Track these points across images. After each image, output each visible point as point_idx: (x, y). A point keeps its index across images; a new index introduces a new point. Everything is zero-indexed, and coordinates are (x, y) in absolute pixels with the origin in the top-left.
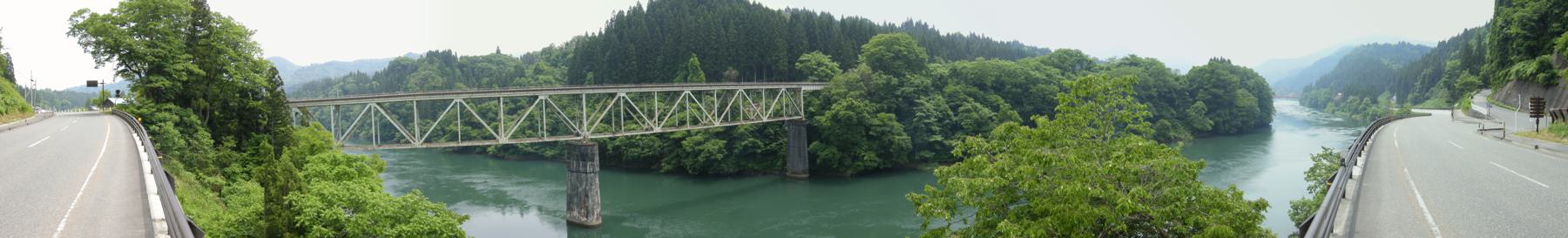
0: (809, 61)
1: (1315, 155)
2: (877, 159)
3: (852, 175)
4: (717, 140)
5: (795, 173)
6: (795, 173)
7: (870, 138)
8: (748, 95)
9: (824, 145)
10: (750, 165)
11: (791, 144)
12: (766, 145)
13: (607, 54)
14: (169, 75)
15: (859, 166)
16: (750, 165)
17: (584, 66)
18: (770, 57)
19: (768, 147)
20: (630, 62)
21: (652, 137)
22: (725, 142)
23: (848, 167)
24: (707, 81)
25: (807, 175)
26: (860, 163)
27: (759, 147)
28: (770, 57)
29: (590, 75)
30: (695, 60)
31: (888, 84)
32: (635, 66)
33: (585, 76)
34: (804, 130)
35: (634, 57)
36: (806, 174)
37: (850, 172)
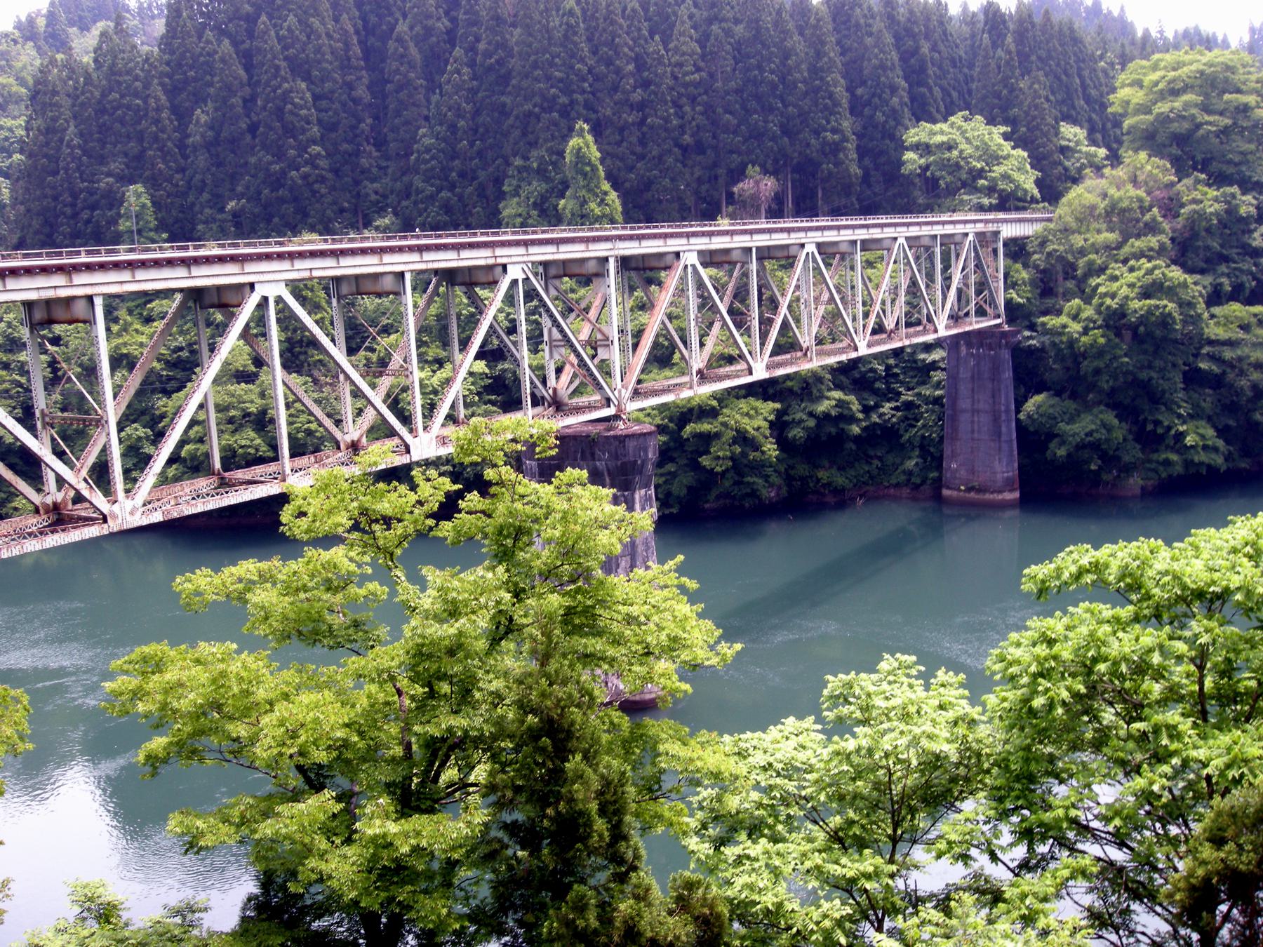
0: (950, 147)
1: (663, 777)
2: (1220, 443)
3: (1145, 493)
4: (758, 403)
5: (980, 490)
6: (980, 490)
7: (1194, 378)
8: (828, 265)
9: (1071, 405)
10: (823, 475)
11: (964, 404)
12: (867, 410)
13: (201, 116)
14: (986, 179)
15: (1167, 463)
16: (823, 475)
17: (102, 160)
18: (817, 133)
19: (875, 418)
20: (303, 149)
21: (192, 433)
22: (778, 406)
23: (1128, 469)
24: (629, 218)
25: (1016, 495)
26: (1174, 457)
27: (852, 419)
28: (817, 133)
29: (136, 196)
30: (582, 142)
31: (1231, 211)
32: (323, 163)
33: (114, 200)
34: (1006, 355)
35: (315, 130)
36: (1011, 491)
37: (1135, 482)
